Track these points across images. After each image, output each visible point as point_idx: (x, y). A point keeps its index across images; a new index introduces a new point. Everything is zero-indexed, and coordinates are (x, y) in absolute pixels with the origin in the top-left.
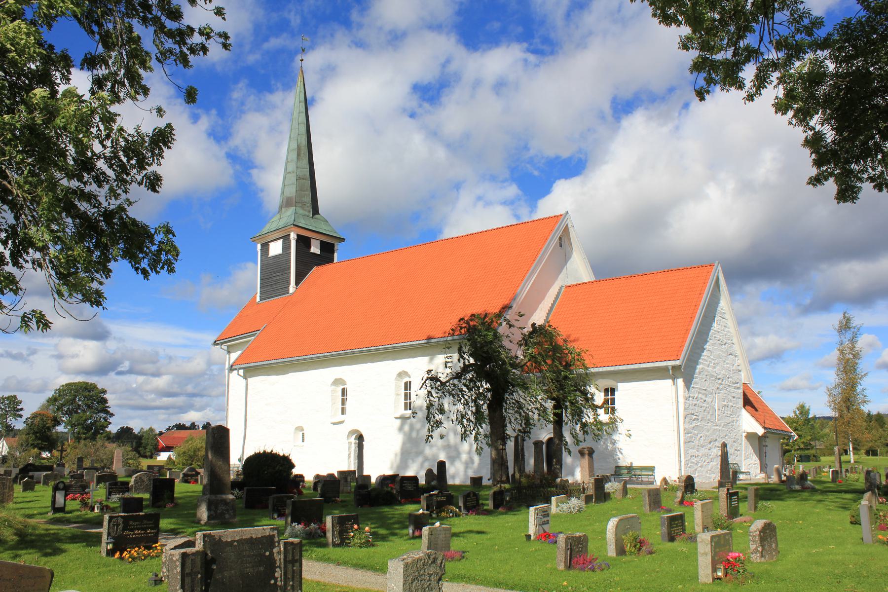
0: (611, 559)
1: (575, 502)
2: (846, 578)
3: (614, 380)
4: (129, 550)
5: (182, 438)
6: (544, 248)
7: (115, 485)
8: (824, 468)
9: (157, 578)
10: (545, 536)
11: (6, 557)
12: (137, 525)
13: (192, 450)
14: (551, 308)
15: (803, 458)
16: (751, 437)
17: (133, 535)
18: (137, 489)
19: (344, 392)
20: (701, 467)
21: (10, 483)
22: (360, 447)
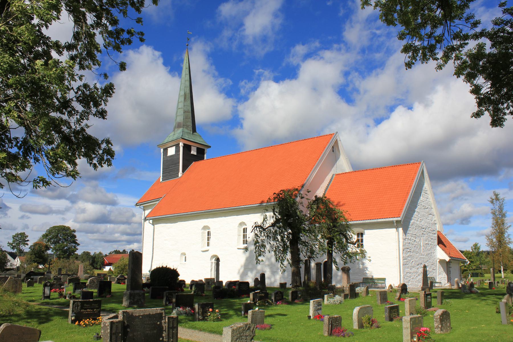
1: (338, 298)
4: (83, 320)
6: (323, 153)
7: (78, 284)
8: (486, 280)
9: (98, 336)
10: (319, 317)
13: (123, 265)
14: (327, 187)
15: (474, 275)
16: (442, 262)
17: (86, 312)
18: (90, 286)
19: (209, 233)
20: (413, 279)
21: (20, 282)
22: (218, 265)
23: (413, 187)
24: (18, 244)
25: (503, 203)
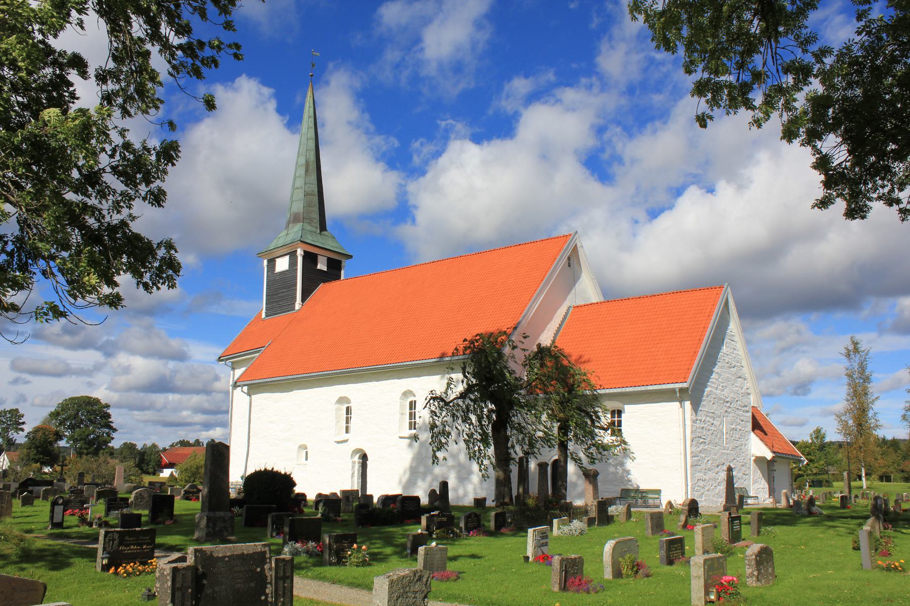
0: (609, 582)
1: (577, 524)
3: (621, 402)
4: (124, 565)
5: (186, 455)
7: (113, 501)
8: (835, 493)
9: (150, 593)
10: (544, 558)
11: (11, 572)
12: (133, 540)
14: (559, 328)
15: (815, 483)
16: (759, 461)
17: (129, 550)
18: (137, 505)
19: (348, 411)
20: (708, 491)
21: (8, 497)
22: (364, 466)
23: (709, 330)
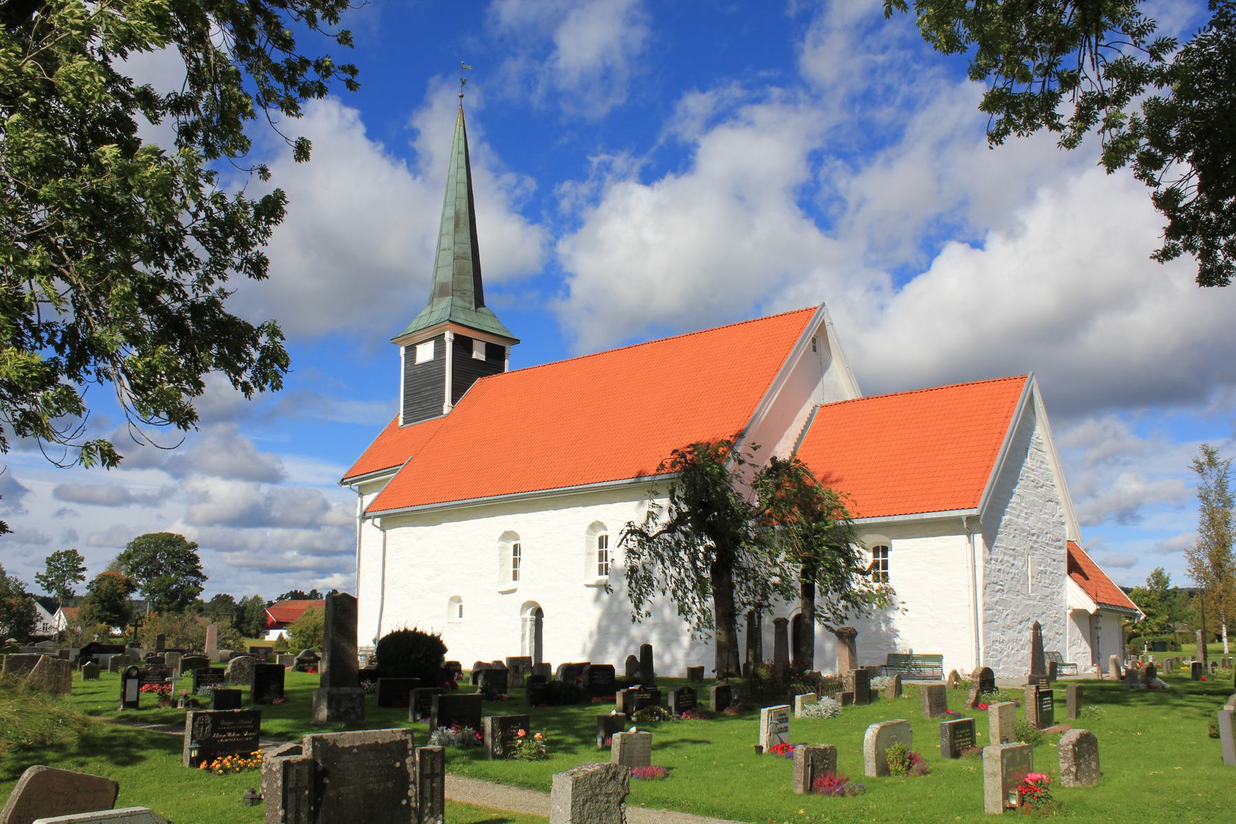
0: (872, 781)
1: (828, 703)
2: (1190, 810)
3: (887, 536)
4: (220, 758)
5: (300, 611)
7: (202, 671)
8: (1184, 659)
9: (254, 796)
12: (230, 725)
13: (312, 628)
14: (801, 436)
15: (1156, 645)
16: (1078, 615)
17: (225, 738)
18: (235, 680)
19: (516, 549)
20: (1008, 656)
24: (62, 578)
25: (1227, 471)
